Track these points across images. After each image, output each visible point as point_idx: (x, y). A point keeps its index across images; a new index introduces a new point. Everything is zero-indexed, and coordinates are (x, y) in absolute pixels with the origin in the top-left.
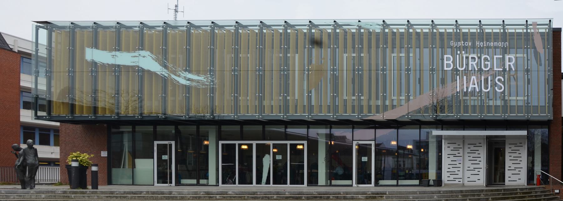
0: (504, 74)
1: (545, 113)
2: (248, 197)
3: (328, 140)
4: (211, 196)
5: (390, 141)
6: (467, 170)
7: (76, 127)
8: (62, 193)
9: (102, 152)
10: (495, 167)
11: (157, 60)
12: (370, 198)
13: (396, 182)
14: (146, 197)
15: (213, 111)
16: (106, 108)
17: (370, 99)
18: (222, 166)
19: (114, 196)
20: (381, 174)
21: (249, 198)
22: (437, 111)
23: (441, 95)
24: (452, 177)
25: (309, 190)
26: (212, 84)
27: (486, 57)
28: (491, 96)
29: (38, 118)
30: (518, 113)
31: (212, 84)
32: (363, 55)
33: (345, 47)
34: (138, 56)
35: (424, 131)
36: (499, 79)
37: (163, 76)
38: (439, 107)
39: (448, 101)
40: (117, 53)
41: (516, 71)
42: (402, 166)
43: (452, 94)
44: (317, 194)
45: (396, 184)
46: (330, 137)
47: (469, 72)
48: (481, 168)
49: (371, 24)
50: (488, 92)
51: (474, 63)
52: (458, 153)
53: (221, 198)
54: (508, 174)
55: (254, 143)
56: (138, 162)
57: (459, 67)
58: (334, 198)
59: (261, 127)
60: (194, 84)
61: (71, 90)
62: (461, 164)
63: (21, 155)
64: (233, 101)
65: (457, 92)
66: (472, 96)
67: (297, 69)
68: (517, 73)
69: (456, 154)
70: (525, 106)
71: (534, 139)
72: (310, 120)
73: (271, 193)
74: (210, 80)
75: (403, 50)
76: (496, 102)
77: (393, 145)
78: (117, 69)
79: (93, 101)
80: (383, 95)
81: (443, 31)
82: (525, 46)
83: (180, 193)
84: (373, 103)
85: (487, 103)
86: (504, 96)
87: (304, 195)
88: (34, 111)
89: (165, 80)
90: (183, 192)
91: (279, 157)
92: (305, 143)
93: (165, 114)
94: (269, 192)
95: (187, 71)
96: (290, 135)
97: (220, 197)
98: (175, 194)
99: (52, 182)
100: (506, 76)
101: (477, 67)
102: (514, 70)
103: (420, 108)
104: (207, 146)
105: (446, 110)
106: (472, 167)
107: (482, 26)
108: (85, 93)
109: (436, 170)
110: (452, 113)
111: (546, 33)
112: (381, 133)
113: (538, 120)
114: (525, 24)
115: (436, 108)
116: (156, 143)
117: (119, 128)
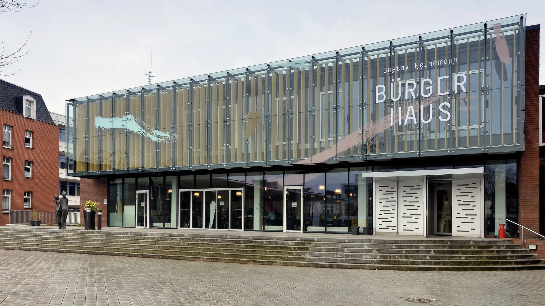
0: (451, 99)
1: (512, 143)
2: (199, 239)
3: (262, 186)
4: (173, 237)
5: (318, 185)
6: (402, 217)
8: (252, 238)
10: (437, 213)
11: (137, 122)
12: (299, 245)
13: (324, 229)
15: (174, 164)
16: (107, 165)
17: (299, 143)
18: (181, 211)
19: (111, 236)
20: (309, 220)
21: (200, 240)
22: (367, 151)
23: (372, 132)
24: (384, 225)
25: (246, 234)
26: (174, 139)
27: (427, 81)
28: (433, 128)
29: (69, 174)
30: (470, 145)
31: (174, 139)
32: (293, 98)
33: (277, 91)
35: (353, 173)
36: (444, 105)
38: (370, 146)
39: (380, 139)
40: (114, 119)
41: (468, 92)
42: (330, 212)
43: (384, 130)
44: (252, 238)
46: (264, 183)
47: (405, 102)
48: (420, 215)
49: (300, 62)
50: (429, 123)
51: (411, 91)
54: (455, 222)
55: (204, 190)
56: (126, 207)
57: (394, 97)
58: (267, 243)
59: (209, 175)
60: (162, 140)
61: (86, 152)
62: (394, 209)
63: (59, 203)
64: (189, 154)
65: (390, 127)
66: (408, 130)
67: (236, 119)
68: (470, 95)
69: (388, 199)
70: (481, 136)
71: (495, 178)
72: (247, 167)
74: (173, 135)
75: (332, 86)
76: (439, 135)
77: (321, 190)
78: (113, 132)
79: (99, 160)
80: (312, 138)
81: (375, 57)
82: (483, 59)
83: (152, 235)
84: (302, 147)
86: (451, 125)
87: (242, 239)
88: (66, 170)
89: (143, 138)
90: (154, 233)
91: (222, 203)
92: (243, 189)
93: (143, 168)
96: (231, 182)
97: (179, 238)
98: (149, 235)
99: (76, 224)
100: (454, 101)
101: (415, 94)
102: (465, 91)
103: (348, 149)
104: (170, 194)
105: (377, 149)
106: (408, 213)
107: (423, 43)
108: (95, 154)
109: (366, 217)
110: (384, 152)
111: (515, 35)
112: (310, 177)
113: (502, 153)
114: (483, 29)
115: (365, 148)
116: (148, 192)
117: (115, 181)
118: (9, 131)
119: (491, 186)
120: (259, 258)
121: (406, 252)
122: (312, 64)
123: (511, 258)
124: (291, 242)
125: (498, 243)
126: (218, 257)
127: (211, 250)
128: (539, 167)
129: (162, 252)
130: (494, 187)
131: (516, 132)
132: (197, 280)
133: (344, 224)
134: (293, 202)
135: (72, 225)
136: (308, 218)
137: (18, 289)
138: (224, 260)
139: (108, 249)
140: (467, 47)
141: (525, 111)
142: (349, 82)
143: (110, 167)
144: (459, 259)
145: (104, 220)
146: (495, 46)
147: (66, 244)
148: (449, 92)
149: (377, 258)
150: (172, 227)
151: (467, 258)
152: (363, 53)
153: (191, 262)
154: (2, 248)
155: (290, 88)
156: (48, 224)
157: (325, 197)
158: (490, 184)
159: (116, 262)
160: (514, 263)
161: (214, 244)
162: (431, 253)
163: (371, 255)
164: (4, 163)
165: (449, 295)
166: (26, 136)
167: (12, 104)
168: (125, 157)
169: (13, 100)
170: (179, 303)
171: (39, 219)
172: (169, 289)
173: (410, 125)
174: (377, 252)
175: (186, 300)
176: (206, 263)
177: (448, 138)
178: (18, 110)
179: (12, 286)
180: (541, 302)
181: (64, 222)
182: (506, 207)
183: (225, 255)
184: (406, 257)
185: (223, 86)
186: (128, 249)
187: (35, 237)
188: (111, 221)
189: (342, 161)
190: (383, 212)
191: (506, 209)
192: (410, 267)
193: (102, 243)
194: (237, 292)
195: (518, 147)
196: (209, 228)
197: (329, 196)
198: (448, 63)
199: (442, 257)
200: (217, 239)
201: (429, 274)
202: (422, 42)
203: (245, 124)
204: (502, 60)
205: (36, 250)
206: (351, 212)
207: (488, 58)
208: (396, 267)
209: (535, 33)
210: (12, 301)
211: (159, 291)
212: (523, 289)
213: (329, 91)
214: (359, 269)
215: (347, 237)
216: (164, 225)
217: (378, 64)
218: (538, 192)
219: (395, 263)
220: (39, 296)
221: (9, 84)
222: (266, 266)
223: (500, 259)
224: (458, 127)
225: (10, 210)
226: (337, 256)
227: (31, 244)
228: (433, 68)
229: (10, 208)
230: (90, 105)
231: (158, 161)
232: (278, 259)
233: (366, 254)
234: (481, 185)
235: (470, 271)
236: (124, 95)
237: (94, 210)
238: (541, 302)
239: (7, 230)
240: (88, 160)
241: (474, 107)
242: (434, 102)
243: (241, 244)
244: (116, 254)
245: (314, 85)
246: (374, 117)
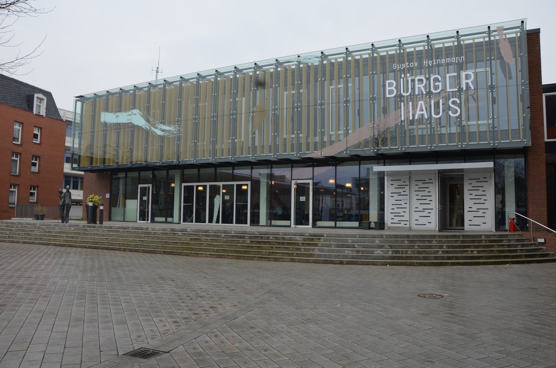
0: (460, 95)
1: (520, 139)
2: (202, 234)
5: (328, 180)
6: (415, 211)
10: (450, 207)
11: (143, 116)
12: (308, 240)
13: (334, 224)
15: (178, 157)
16: (110, 159)
17: (308, 136)
18: (184, 205)
20: (318, 214)
21: (203, 236)
22: (378, 144)
24: (396, 220)
25: (251, 229)
26: (179, 132)
27: (436, 78)
28: (443, 123)
29: (73, 169)
30: (480, 140)
32: (302, 91)
33: (286, 85)
35: (364, 167)
36: (453, 101)
38: (381, 139)
40: (119, 114)
41: (476, 89)
42: (341, 206)
43: (395, 124)
44: (258, 233)
46: (271, 176)
48: (433, 209)
49: (310, 57)
50: (440, 118)
51: (421, 86)
52: (403, 191)
54: (467, 216)
55: (208, 184)
57: (404, 92)
58: (273, 238)
60: (167, 134)
61: (91, 146)
62: (407, 203)
64: (193, 147)
65: (401, 121)
66: (420, 124)
67: (243, 112)
68: (477, 92)
69: (401, 193)
70: (490, 131)
71: (504, 172)
72: (253, 161)
75: (342, 81)
76: (450, 129)
77: (331, 184)
78: (118, 126)
82: (488, 58)
83: (153, 229)
84: (311, 140)
86: (461, 120)
87: (247, 234)
89: (147, 133)
92: (249, 183)
93: (146, 162)
96: (237, 176)
97: (181, 233)
100: (463, 97)
101: (425, 89)
102: (473, 88)
103: (359, 143)
104: (173, 188)
105: (389, 142)
106: (421, 207)
107: (430, 42)
108: (99, 148)
109: (378, 211)
110: (396, 146)
112: (320, 171)
114: (487, 31)
115: (377, 141)
116: (150, 186)
117: (117, 175)
118: (19, 128)
119: (501, 180)
120: (265, 254)
121: (418, 247)
122: (321, 59)
123: (521, 252)
125: (508, 237)
126: (222, 253)
127: (215, 246)
128: (545, 162)
130: (503, 181)
131: (523, 128)
132: (200, 276)
133: (355, 219)
134: (301, 196)
135: (75, 219)
136: (317, 213)
137: (21, 282)
138: (228, 256)
139: (109, 244)
140: (472, 47)
141: (531, 108)
143: (114, 162)
144: (471, 253)
145: (106, 214)
146: (499, 46)
148: (458, 88)
149: (389, 253)
150: (174, 222)
151: (479, 252)
152: (372, 50)
153: (193, 258)
154: (7, 241)
155: (299, 82)
156: (51, 218)
157: (335, 191)
158: (500, 178)
159: (117, 257)
160: (523, 256)
161: (218, 239)
162: (444, 248)
163: (383, 251)
164: (13, 158)
165: (461, 290)
166: (35, 132)
167: (24, 102)
168: (128, 151)
169: (25, 97)
170: (180, 300)
171: (43, 213)
172: (170, 285)
173: (421, 120)
174: (389, 247)
175: (188, 296)
176: (208, 259)
177: (458, 133)
178: (29, 108)
179: (15, 279)
180: (550, 295)
181: (67, 216)
182: (516, 201)
184: (419, 252)
185: (230, 80)
186: (128, 244)
187: (39, 230)
188: (112, 215)
189: (353, 154)
190: (395, 207)
191: (516, 203)
192: (422, 262)
193: (103, 237)
194: (241, 289)
195: (525, 142)
196: (213, 222)
197: (339, 190)
198: (456, 61)
199: (454, 252)
201: (442, 269)
202: (430, 41)
203: (252, 117)
204: (506, 59)
205: (39, 244)
206: (362, 206)
207: (493, 57)
208: (408, 263)
209: (536, 36)
210: (15, 294)
211: (160, 287)
212: (532, 282)
213: (339, 85)
214: (370, 265)
215: (360, 232)
216: (166, 220)
217: (387, 60)
218: (545, 186)
219: (407, 258)
220: (41, 290)
221: (22, 83)
222: (272, 262)
223: (510, 253)
224: (468, 122)
225: (16, 204)
226: (347, 252)
227: (35, 238)
228: (442, 65)
229: (16, 202)
230: (97, 101)
231: (162, 154)
233: (377, 249)
234: (491, 179)
235: (482, 265)
236: (131, 90)
237: (96, 204)
238: (550, 295)
239: (12, 223)
240: (92, 154)
241: (482, 103)
242: (444, 97)
243: (246, 240)
244: (117, 249)
245: (323, 79)
246: (385, 111)
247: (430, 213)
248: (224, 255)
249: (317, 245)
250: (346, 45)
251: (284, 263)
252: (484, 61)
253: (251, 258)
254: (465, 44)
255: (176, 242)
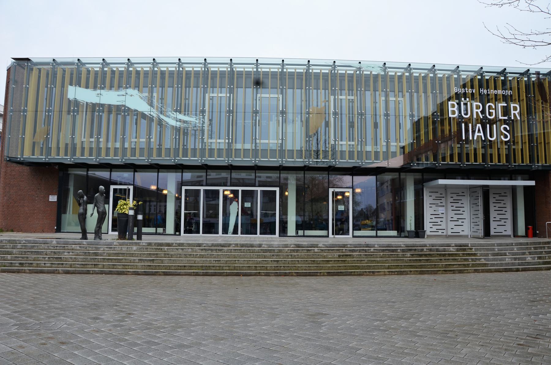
2: (346, 250)
7: (23, 168)
8: (147, 244)
9: (50, 196)
14: (243, 250)
17: (107, 141)
21: (347, 251)
30: (244, 157)
34: (125, 94)
37: (151, 117)
44: (404, 246)
45: (375, 235)
49: (373, 66)
52: (440, 203)
53: (319, 251)
58: (428, 250)
73: (361, 246)
76: (236, 145)
80: (72, 137)
81: (165, 69)
85: (209, 146)
94: (358, 244)
95: (178, 112)
97: (318, 250)
120: (441, 267)
124: (452, 249)
129: (318, 268)
138: (411, 271)
142: (402, 92)
147: (143, 262)
152: (179, 64)
161: (373, 255)
183: (403, 266)
186: (264, 266)
187: (73, 252)
190: (433, 217)
200: (369, 248)
227: (82, 264)
232: (461, 266)
247: (463, 222)
248: (405, 271)
249: (476, 255)
250: (154, 56)
251: (468, 274)
252: (225, 87)
253: (436, 272)
254: (220, 71)
255: (327, 261)
